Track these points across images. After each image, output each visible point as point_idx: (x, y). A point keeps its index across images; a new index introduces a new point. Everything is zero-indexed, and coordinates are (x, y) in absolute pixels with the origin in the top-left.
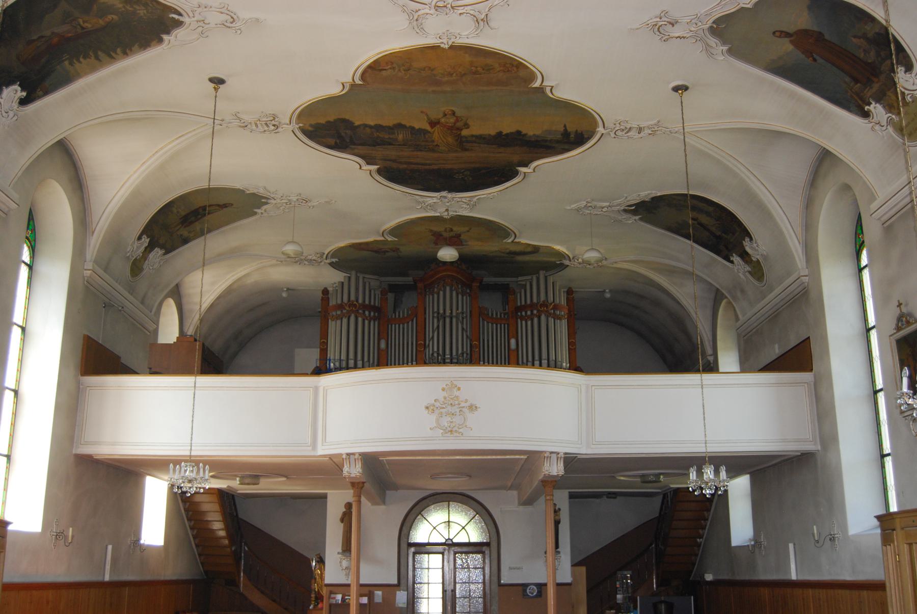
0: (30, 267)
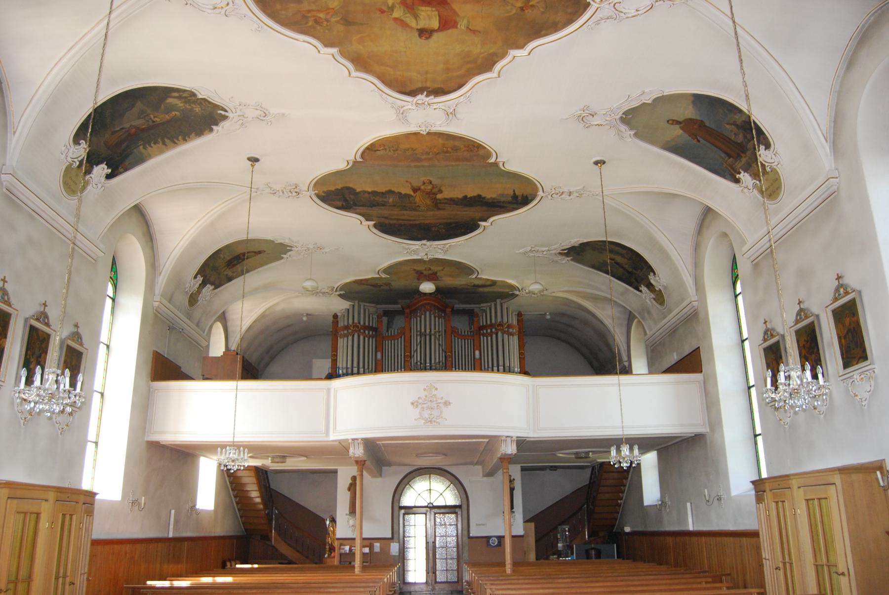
0: (113, 300)
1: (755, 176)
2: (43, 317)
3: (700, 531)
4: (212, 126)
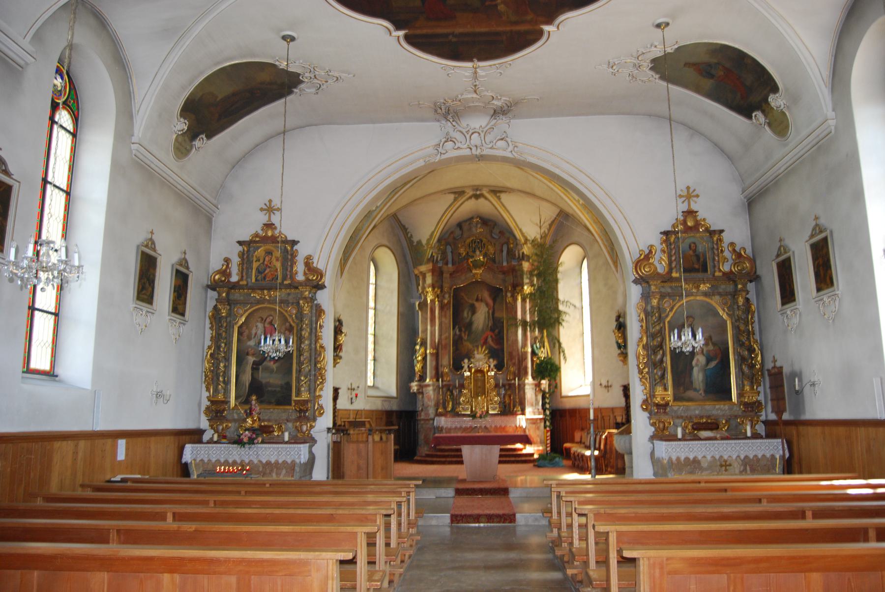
0: (74, 135)
1: (766, 116)
2: (184, 262)
3: (43, 432)
4: (415, 244)
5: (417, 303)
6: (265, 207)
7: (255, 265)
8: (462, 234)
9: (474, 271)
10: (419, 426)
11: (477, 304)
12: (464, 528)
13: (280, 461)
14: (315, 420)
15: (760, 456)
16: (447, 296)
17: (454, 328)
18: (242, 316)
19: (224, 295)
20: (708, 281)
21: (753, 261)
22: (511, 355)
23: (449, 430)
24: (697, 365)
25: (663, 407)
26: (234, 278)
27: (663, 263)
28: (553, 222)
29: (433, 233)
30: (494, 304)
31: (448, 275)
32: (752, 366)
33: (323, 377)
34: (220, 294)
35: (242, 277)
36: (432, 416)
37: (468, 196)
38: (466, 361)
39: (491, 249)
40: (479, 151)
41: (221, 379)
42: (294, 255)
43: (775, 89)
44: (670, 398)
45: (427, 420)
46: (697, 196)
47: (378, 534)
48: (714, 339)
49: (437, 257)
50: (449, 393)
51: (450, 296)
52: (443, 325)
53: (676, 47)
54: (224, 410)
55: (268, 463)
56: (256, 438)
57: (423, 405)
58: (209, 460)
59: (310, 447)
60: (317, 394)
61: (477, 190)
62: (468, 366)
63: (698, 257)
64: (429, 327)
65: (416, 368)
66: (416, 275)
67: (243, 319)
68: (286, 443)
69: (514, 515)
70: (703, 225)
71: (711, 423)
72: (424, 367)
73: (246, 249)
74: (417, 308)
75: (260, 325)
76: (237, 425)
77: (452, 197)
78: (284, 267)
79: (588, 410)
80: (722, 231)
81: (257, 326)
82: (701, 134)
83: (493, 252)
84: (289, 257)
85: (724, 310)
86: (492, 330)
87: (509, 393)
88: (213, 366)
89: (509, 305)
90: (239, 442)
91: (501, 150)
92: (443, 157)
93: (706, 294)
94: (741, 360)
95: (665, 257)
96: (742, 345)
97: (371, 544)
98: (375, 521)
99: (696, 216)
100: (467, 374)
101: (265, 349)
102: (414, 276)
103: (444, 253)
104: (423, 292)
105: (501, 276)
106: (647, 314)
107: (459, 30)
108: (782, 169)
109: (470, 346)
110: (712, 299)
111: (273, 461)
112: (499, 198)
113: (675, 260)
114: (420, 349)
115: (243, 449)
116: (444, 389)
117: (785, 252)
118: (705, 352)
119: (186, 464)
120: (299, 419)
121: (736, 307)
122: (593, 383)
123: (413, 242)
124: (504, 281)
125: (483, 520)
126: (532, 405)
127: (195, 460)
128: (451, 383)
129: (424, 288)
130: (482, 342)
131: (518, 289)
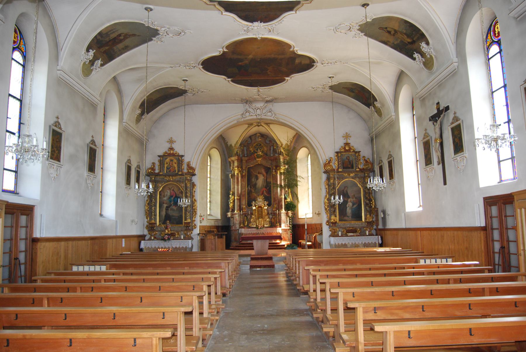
0: (24, 66)
4: (229, 146)
5: (230, 175)
6: (169, 140)
7: (166, 166)
8: (251, 142)
9: (257, 159)
10: (232, 233)
11: (259, 175)
12: (255, 270)
13: (181, 247)
14: (193, 230)
15: (370, 243)
16: (244, 171)
17: (248, 186)
18: (161, 187)
19: (153, 178)
20: (354, 172)
21: (372, 164)
22: (275, 200)
23: (246, 234)
24: (349, 207)
25: (335, 223)
26: (157, 171)
27: (336, 165)
28: (295, 136)
29: (238, 141)
30: (267, 175)
31: (245, 162)
32: (371, 207)
33: (196, 212)
34: (151, 178)
35: (160, 170)
36: (238, 228)
37: (254, 125)
38: (254, 202)
39: (265, 149)
40: (260, 117)
41: (153, 214)
42: (182, 161)
43: (376, 101)
44: (337, 219)
45: (236, 230)
46: (350, 137)
47: (204, 297)
48: (356, 196)
49: (240, 153)
50: (245, 217)
51: (246, 172)
52: (243, 185)
53: (338, 83)
54: (155, 227)
55: (176, 248)
56: (170, 238)
57: (233, 223)
58: (152, 247)
59: (192, 241)
60: (193, 219)
61: (259, 123)
62: (255, 205)
63: (350, 162)
64: (236, 186)
65: (230, 206)
66: (229, 161)
67: (161, 188)
68: (182, 240)
69: (274, 265)
70: (352, 149)
71: (354, 230)
72: (234, 205)
73: (162, 159)
74: (230, 177)
75: (169, 191)
76: (160, 233)
77: (247, 126)
78: (179, 167)
79: (304, 225)
80: (360, 152)
81: (167, 192)
82: (353, 110)
83: (266, 150)
84: (181, 162)
85: (360, 184)
86: (266, 188)
87: (274, 217)
88: (149, 208)
89: (274, 176)
90: (163, 239)
91: (269, 117)
92: (245, 119)
93: (353, 178)
94: (366, 205)
95: (337, 163)
96: (366, 198)
97: (201, 303)
98: (202, 289)
99: (349, 145)
100: (254, 208)
101: (181, 204)
102: (228, 162)
103: (243, 151)
104: (233, 170)
105: (270, 162)
106: (329, 186)
107: (252, 79)
108: (381, 130)
109: (256, 195)
110: (355, 180)
111: (178, 247)
112: (269, 126)
113: (340, 164)
114: (232, 197)
115: (165, 242)
116: (243, 216)
117: (381, 163)
118: (352, 201)
119: (142, 249)
120: (186, 230)
121: (365, 183)
122: (313, 213)
123: (228, 145)
124: (271, 164)
125: (262, 267)
126: (285, 223)
127: (145, 247)
128: (246, 212)
129: (233, 168)
130: (261, 193)
131: (278, 168)
